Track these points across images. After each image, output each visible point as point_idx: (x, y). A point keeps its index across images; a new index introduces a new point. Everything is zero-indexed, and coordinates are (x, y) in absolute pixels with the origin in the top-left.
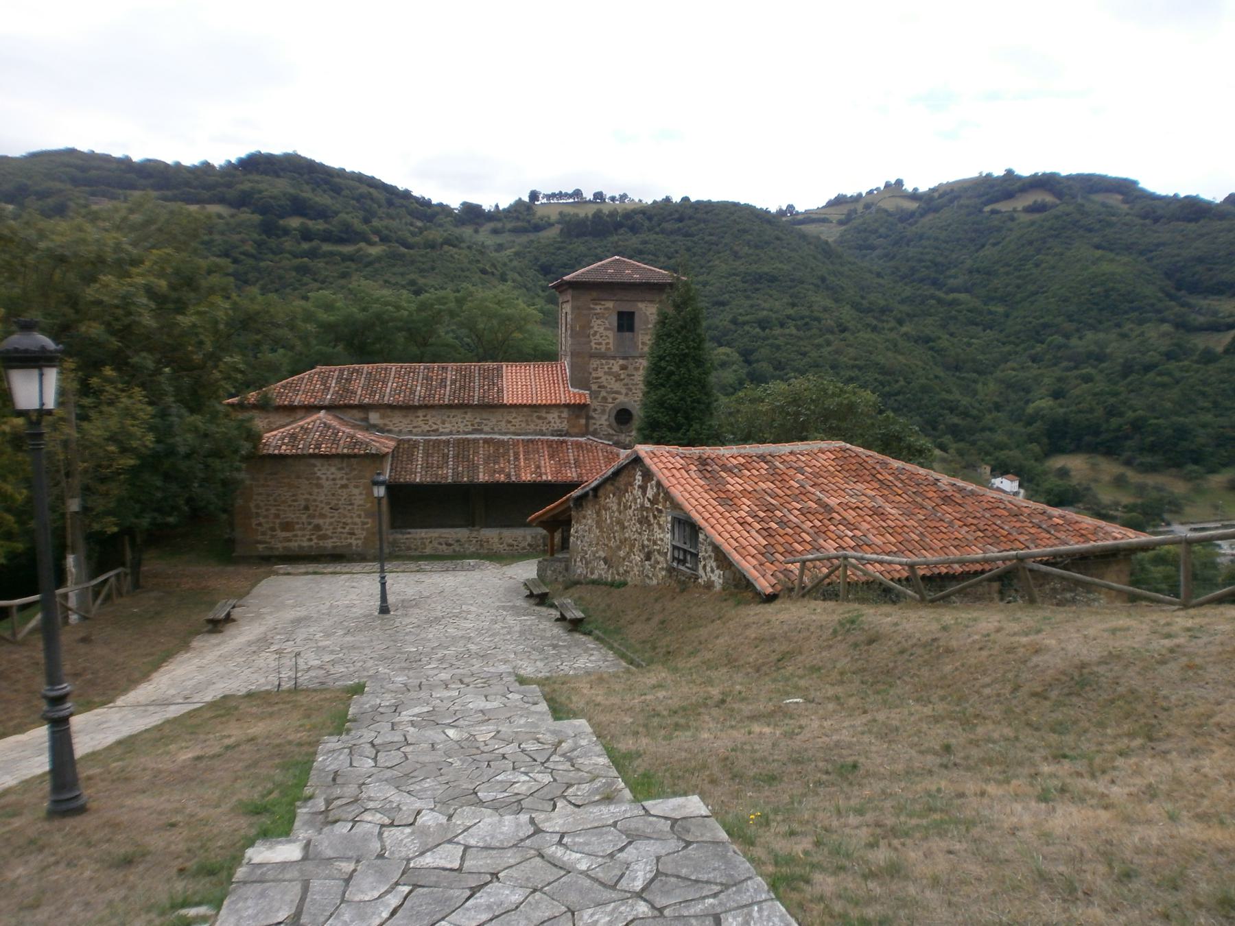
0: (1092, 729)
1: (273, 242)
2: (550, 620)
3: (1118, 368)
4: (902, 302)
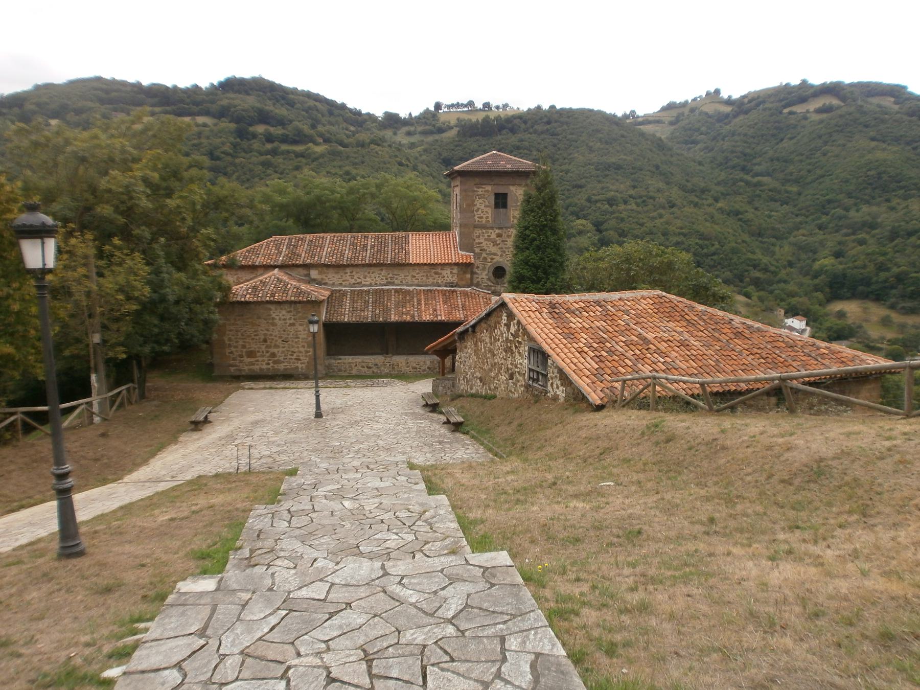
0: (823, 508)
1: (245, 144)
2: (439, 423)
3: (887, 234)
4: (718, 184)
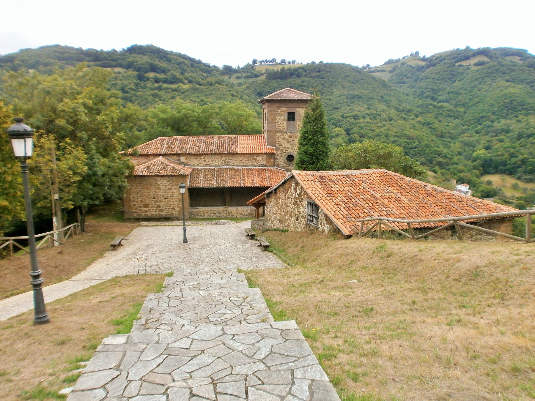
1: (142, 84)
3: (516, 136)
4: (418, 107)
